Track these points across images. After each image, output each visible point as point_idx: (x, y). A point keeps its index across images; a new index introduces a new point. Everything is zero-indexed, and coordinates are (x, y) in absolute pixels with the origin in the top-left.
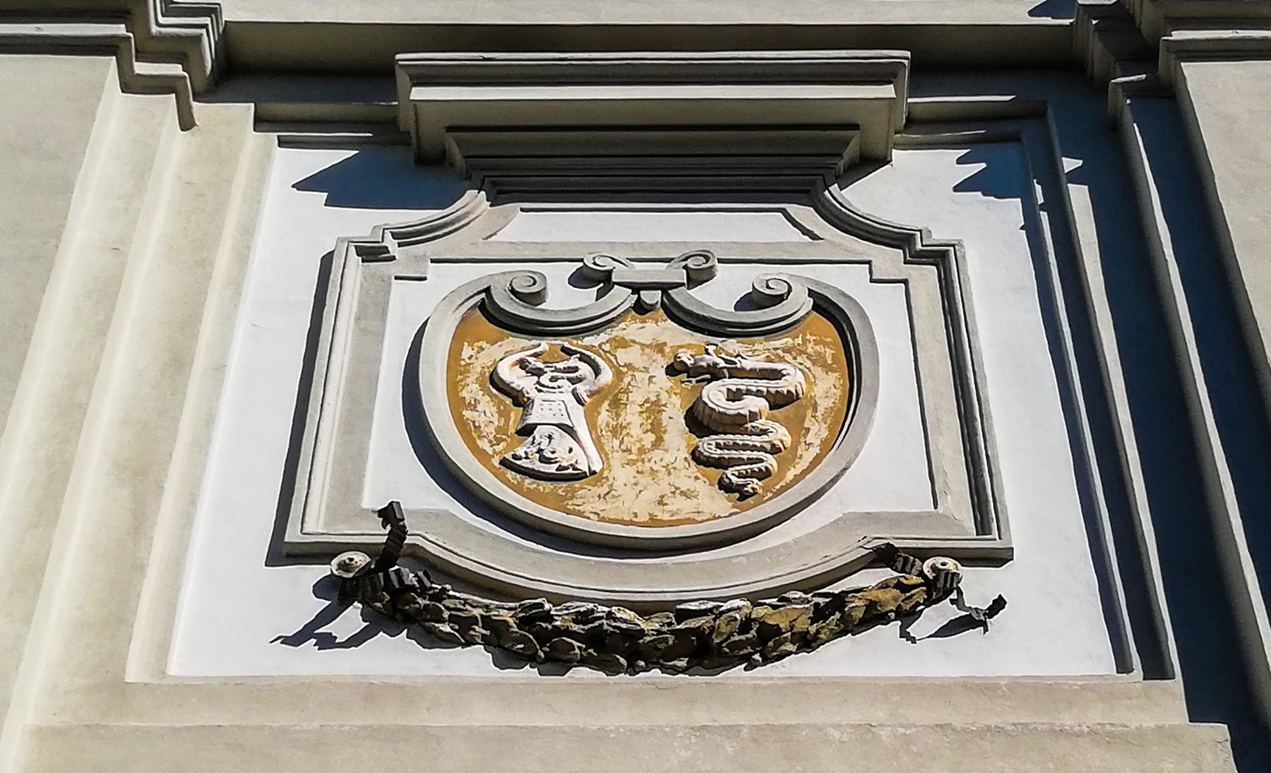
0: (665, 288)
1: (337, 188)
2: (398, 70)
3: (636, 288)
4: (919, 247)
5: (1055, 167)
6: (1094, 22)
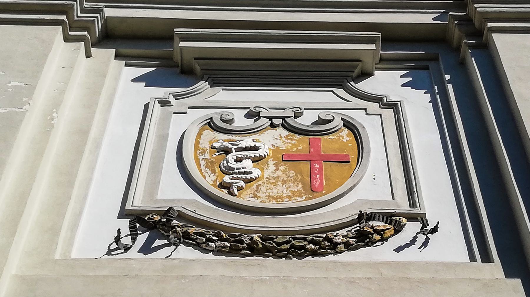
0: (283, 118)
1: (149, 80)
2: (175, 36)
3: (270, 118)
4: (385, 102)
5: (443, 79)
6: (456, 22)
